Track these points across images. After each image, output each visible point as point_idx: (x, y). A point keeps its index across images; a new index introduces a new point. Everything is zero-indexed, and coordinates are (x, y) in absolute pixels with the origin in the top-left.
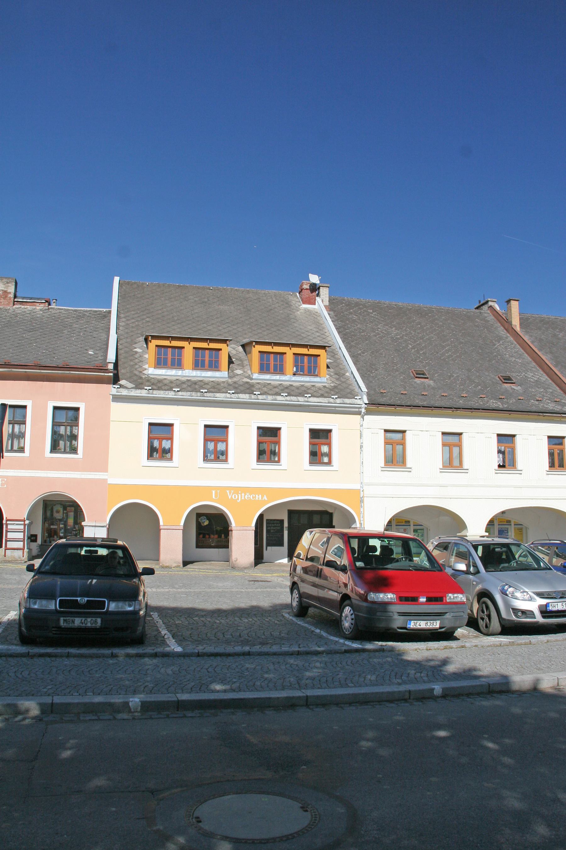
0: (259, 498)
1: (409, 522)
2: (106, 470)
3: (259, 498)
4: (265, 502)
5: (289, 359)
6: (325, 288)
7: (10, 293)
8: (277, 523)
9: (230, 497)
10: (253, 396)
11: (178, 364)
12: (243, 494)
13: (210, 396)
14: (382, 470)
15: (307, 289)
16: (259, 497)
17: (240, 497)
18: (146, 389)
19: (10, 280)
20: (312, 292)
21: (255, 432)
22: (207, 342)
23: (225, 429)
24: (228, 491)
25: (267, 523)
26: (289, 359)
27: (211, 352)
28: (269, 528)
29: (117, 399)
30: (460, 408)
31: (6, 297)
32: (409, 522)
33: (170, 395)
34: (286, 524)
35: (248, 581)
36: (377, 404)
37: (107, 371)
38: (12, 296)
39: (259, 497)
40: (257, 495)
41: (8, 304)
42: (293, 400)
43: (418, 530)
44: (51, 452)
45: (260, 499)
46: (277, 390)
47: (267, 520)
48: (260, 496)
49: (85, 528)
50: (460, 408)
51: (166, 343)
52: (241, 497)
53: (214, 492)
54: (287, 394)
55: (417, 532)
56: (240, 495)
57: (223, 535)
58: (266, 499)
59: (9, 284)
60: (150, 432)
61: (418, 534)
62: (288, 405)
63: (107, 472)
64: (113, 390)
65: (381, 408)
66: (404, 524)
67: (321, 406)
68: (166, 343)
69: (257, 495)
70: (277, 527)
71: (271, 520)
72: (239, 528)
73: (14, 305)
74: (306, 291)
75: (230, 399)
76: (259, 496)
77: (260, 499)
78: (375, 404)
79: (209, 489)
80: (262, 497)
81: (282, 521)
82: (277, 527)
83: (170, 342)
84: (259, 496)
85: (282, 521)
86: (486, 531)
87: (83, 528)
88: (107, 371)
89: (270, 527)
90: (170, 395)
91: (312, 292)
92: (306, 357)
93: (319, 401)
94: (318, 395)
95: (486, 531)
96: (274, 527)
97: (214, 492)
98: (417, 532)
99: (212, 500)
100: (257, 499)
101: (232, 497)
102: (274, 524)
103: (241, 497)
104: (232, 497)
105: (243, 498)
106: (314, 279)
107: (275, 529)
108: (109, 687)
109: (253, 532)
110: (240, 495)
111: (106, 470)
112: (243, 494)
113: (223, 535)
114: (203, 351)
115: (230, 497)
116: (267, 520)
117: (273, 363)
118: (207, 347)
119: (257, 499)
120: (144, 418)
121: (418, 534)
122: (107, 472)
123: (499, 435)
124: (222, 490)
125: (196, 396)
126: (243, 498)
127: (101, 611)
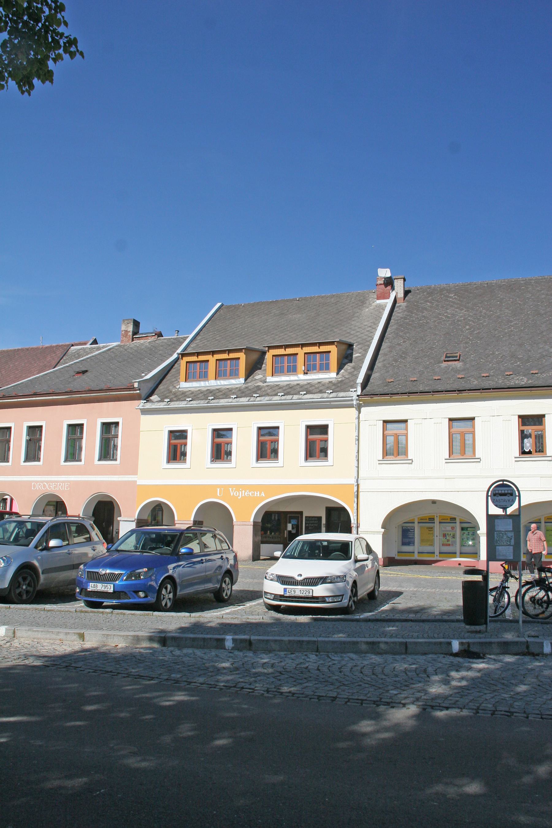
0: (257, 495)
1: (455, 519)
2: (135, 472)
3: (257, 495)
4: (263, 499)
5: (300, 359)
6: (399, 280)
7: (129, 331)
8: (315, 520)
9: (232, 494)
10: (252, 399)
11: (204, 376)
12: (243, 492)
13: (215, 403)
14: (516, 461)
15: (381, 284)
16: (257, 494)
17: (241, 494)
18: (352, 391)
19: (130, 321)
20: (386, 286)
21: (515, 421)
22: (282, 348)
23: (277, 430)
24: (230, 489)
25: (306, 520)
26: (300, 359)
27: (289, 357)
28: (307, 525)
29: (145, 412)
30: (465, 390)
31: (127, 335)
32: (455, 519)
33: (276, 399)
34: (324, 521)
35: (355, 582)
36: (370, 395)
37: (134, 389)
38: (131, 334)
39: (257, 494)
40: (255, 492)
41: (128, 341)
42: (288, 399)
43: (468, 528)
44: (100, 459)
45: (258, 495)
46: (290, 390)
47: (306, 517)
48: (258, 492)
49: (121, 523)
50: (465, 390)
51: (225, 356)
52: (242, 494)
53: (218, 489)
54: (305, 392)
55: (467, 530)
56: (240, 492)
57: (269, 532)
58: (264, 496)
59: (129, 325)
60: (384, 429)
61: (469, 533)
62: (282, 404)
63: (137, 475)
64: (141, 404)
65: (412, 396)
66: (449, 521)
67: (313, 402)
68: (225, 356)
69: (255, 492)
70: (315, 523)
71: (310, 517)
72: (239, 523)
73: (133, 340)
74: (380, 286)
75: (232, 404)
76: (257, 493)
77: (258, 495)
78: (368, 395)
79: (214, 487)
80: (260, 494)
81: (320, 518)
82: (315, 523)
83: (319, 348)
84: (257, 493)
85: (320, 518)
86: (382, 528)
87: (479, 537)
88: (134, 389)
89: (308, 524)
90: (182, 404)
91: (386, 286)
92: (318, 355)
93: (312, 397)
94: (264, 394)
95: (382, 528)
96: (312, 524)
97: (218, 489)
98: (467, 530)
99: (218, 498)
100: (255, 495)
101: (233, 494)
102: (312, 520)
103: (242, 494)
104: (233, 494)
105: (243, 495)
106: (384, 273)
107: (312, 526)
108: (232, 688)
109: (252, 526)
110: (240, 492)
111: (135, 472)
112: (243, 492)
113: (269, 532)
114: (282, 357)
115: (232, 494)
116: (306, 517)
117: (317, 363)
118: (228, 357)
119: (255, 495)
120: (165, 426)
121: (469, 533)
122: (137, 475)
123: (520, 417)
124: (226, 487)
125: (202, 403)
126: (243, 495)
127: (324, 618)
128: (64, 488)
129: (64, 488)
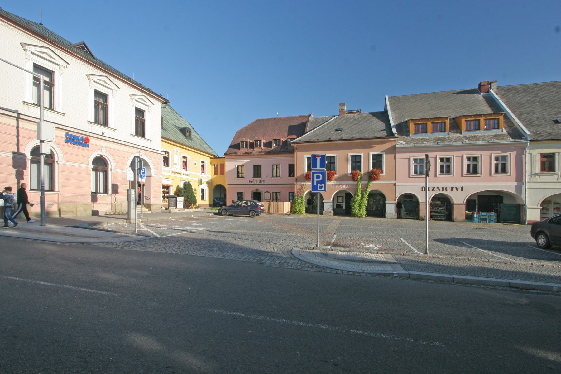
31: (343, 111)
34: (477, 202)
85: (475, 201)
128: (352, 187)
129: (352, 187)
